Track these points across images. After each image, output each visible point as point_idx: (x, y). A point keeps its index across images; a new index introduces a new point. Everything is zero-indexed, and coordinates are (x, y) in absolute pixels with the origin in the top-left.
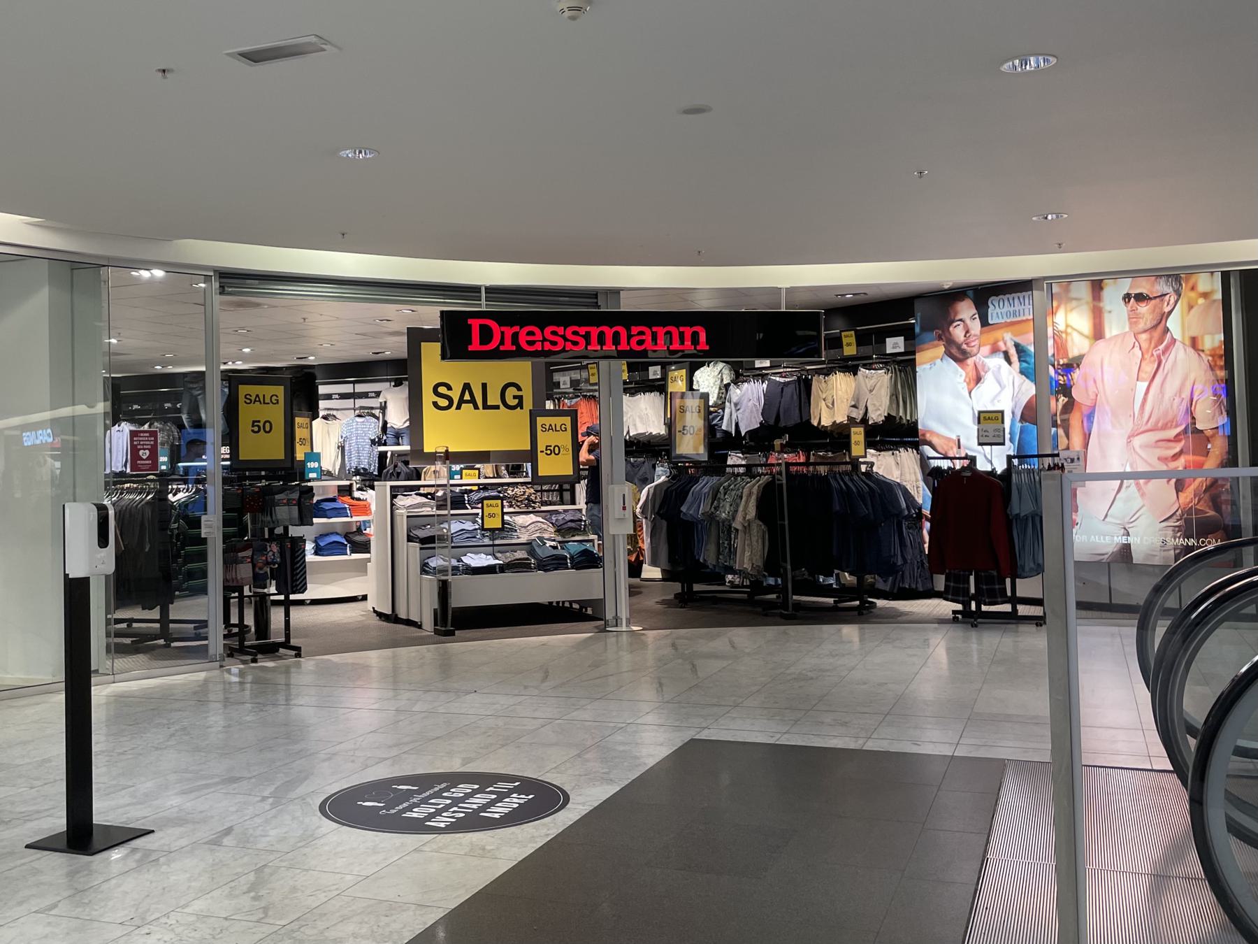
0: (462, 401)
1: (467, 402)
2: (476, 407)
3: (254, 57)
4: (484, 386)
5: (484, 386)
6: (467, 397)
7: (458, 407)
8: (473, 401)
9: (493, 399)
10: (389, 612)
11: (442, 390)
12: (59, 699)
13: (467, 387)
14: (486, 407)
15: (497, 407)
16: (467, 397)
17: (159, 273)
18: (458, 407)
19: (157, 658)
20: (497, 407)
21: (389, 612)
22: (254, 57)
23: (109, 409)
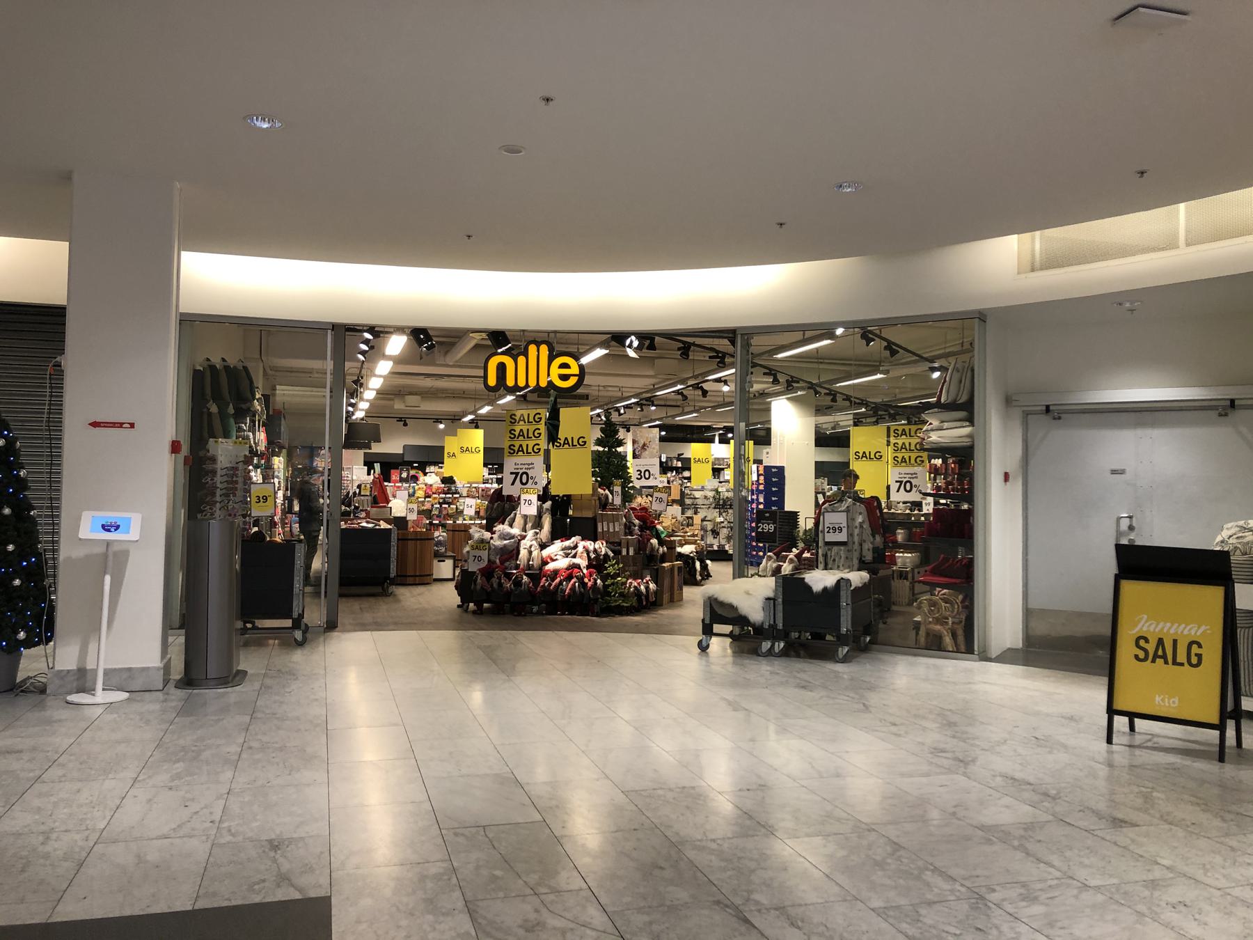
0: (1156, 656)
1: (1160, 657)
2: (1166, 662)
3: (95, 424)
4: (1175, 642)
5: (1175, 642)
6: (1160, 653)
7: (1154, 661)
8: (1164, 657)
9: (1182, 657)
10: (1137, 720)
11: (1142, 643)
12: (1115, 729)
13: (1160, 642)
14: (1175, 663)
15: (1182, 664)
16: (1160, 653)
17: (599, 353)
18: (1154, 661)
19: (731, 607)
20: (1182, 664)
21: (1137, 720)
22: (95, 424)
23: (344, 473)
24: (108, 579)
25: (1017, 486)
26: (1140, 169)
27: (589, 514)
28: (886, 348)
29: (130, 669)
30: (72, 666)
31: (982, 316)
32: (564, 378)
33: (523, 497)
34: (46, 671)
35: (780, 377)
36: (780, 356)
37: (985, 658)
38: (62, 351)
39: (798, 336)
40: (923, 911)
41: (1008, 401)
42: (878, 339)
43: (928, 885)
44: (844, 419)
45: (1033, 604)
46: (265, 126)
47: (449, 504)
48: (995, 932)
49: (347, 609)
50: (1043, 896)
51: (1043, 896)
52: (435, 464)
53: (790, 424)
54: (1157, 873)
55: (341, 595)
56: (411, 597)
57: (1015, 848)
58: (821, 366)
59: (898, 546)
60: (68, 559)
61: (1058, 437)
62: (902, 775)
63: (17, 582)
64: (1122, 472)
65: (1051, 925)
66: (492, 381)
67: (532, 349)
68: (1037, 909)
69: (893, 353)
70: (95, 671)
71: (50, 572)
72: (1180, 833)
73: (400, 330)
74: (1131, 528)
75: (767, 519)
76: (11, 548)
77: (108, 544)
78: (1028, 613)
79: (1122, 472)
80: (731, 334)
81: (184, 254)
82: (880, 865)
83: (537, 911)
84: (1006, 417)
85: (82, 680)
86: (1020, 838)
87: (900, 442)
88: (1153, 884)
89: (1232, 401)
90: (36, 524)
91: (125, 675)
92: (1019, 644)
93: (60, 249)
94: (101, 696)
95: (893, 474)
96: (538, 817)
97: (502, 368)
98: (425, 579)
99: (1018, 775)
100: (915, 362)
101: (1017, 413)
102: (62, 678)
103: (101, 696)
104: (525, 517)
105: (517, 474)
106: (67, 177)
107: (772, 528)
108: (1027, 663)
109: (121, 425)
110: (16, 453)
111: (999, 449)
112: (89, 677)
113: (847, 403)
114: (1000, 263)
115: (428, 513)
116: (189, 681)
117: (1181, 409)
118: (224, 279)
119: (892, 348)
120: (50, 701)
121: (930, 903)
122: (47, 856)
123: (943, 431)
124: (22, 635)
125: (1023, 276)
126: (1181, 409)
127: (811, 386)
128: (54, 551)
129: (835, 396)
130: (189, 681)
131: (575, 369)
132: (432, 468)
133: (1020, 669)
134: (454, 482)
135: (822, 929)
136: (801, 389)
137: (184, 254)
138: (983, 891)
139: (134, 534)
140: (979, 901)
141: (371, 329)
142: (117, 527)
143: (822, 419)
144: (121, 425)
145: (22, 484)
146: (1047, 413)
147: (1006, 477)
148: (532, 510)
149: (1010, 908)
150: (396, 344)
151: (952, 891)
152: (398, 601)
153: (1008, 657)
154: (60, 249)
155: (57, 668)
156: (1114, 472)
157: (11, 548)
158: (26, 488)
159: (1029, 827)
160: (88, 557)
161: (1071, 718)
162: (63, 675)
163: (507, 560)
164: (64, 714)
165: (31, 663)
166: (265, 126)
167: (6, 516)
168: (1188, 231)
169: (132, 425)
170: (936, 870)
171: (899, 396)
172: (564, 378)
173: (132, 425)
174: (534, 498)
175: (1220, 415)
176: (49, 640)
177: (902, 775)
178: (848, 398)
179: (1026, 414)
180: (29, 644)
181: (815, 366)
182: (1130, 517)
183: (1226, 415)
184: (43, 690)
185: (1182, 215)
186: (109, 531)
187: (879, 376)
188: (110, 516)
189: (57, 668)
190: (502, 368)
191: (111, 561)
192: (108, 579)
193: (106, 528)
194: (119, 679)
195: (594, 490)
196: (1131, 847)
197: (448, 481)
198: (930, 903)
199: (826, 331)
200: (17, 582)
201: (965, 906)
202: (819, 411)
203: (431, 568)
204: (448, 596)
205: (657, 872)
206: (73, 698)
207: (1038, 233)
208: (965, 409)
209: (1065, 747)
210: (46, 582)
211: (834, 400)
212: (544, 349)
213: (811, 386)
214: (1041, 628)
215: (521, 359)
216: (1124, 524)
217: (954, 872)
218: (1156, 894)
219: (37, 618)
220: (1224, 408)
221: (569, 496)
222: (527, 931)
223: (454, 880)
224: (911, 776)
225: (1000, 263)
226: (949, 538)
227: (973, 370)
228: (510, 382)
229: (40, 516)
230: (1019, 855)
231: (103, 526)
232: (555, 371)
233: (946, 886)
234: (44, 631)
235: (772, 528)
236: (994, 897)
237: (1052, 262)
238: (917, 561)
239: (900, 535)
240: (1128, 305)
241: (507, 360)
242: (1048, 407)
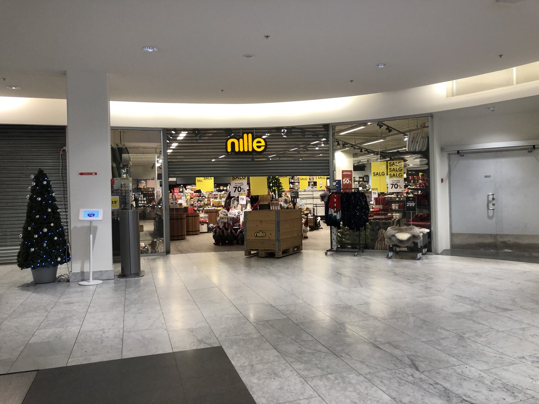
3: (81, 174)
22: (81, 174)
24: (91, 236)
25: (446, 183)
26: (499, 54)
27: (267, 203)
28: (386, 129)
29: (101, 271)
30: (79, 271)
31: (431, 115)
32: (259, 147)
33: (240, 197)
34: (68, 273)
35: (340, 142)
36: (341, 134)
37: (438, 254)
38: (65, 145)
39: (351, 126)
40: (441, 341)
41: (442, 149)
42: (384, 126)
43: (440, 333)
44: (363, 159)
45: (453, 232)
46: (151, 50)
47: (201, 201)
48: (469, 346)
49: (173, 246)
50: (484, 335)
51: (484, 335)
52: (190, 185)
53: (342, 162)
54: (524, 326)
55: (171, 240)
56: (192, 240)
57: (469, 320)
58: (356, 137)
59: (393, 211)
60: (75, 227)
61: (463, 162)
62: (418, 297)
63: (56, 238)
64: (489, 177)
65: (490, 343)
66: (229, 150)
67: (245, 135)
68: (483, 339)
69: (390, 131)
70: (89, 272)
71: (66, 234)
72: (529, 312)
73: (184, 130)
74: (493, 199)
75: (411, 200)
76: (52, 225)
77: (91, 222)
78: (452, 235)
79: (489, 177)
80: (326, 127)
81: (111, 102)
82: (421, 327)
83: (300, 347)
84: (442, 156)
85: (83, 276)
86: (469, 316)
87: (392, 168)
88: (523, 329)
89: (534, 146)
90: (60, 215)
91: (99, 274)
92: (449, 247)
93: (63, 102)
94: (92, 282)
95: (388, 180)
96: (286, 317)
97: (233, 144)
98: (196, 232)
99: (462, 295)
100: (397, 134)
101: (446, 154)
102: (75, 276)
103: (92, 282)
104: (242, 205)
105: (236, 188)
106: (65, 74)
107: (413, 204)
108: (452, 254)
109: (91, 174)
110: (50, 187)
111: (440, 168)
112: (85, 275)
113: (366, 152)
114: (441, 93)
115: (192, 205)
116: (123, 275)
117: (513, 150)
118: (126, 112)
119: (389, 129)
120: (72, 284)
121: (443, 339)
122: (107, 337)
123: (413, 162)
124: (59, 259)
125: (449, 98)
126: (513, 150)
127: (352, 146)
128: (67, 226)
129: (361, 149)
130: (123, 275)
131: (263, 143)
132: (189, 187)
133: (449, 257)
134: (201, 192)
135: (406, 349)
136: (348, 147)
137: (111, 102)
138: (461, 334)
139: (100, 217)
140: (461, 337)
141: (175, 130)
142: (94, 215)
143: (356, 159)
144: (91, 174)
145: (54, 199)
146: (459, 154)
147: (442, 180)
148: (244, 202)
149: (473, 339)
150: (182, 136)
151: (450, 334)
152: (188, 241)
153: (445, 253)
154: (63, 102)
155: (73, 272)
156: (486, 177)
157: (52, 225)
158: (55, 201)
159: (472, 312)
160: (82, 228)
161: (477, 274)
162: (75, 274)
163: (235, 223)
164: (80, 289)
165: (62, 270)
166: (151, 50)
167: (49, 212)
168: (517, 78)
169: (96, 174)
170: (441, 328)
171: (387, 148)
172: (259, 147)
173: (96, 174)
174: (245, 197)
175: (529, 152)
176: (68, 261)
177: (418, 297)
178: (366, 150)
179: (449, 155)
180: (61, 263)
181: (354, 137)
182: (493, 195)
183: (531, 152)
184: (68, 281)
185: (514, 72)
186: (90, 216)
187: (381, 140)
188: (91, 210)
189: (73, 272)
190: (233, 144)
191: (91, 230)
192: (91, 236)
193: (89, 215)
194: (98, 275)
195: (269, 193)
196: (512, 317)
197: (199, 191)
198: (443, 339)
199: (364, 123)
200: (56, 238)
201: (456, 339)
202: (355, 155)
203: (199, 228)
204: (209, 238)
205: (338, 333)
206: (81, 283)
207: (454, 81)
208: (425, 154)
209: (477, 284)
210: (66, 238)
211: (361, 151)
212: (250, 135)
213: (352, 146)
214: (457, 241)
215: (241, 140)
216: (491, 198)
217: (448, 329)
218: (525, 332)
219: (64, 252)
220: (531, 149)
221: (258, 196)
222: (299, 354)
223: (264, 339)
224: (421, 297)
225: (441, 93)
226: (418, 207)
227: (428, 138)
228: (237, 150)
229: (61, 212)
230: (471, 322)
231: (88, 215)
232: (255, 145)
233: (448, 333)
234: (66, 258)
235: (413, 204)
236: (467, 335)
237: (460, 92)
238: (401, 217)
239: (394, 206)
240: (492, 109)
241: (235, 141)
242: (458, 151)
